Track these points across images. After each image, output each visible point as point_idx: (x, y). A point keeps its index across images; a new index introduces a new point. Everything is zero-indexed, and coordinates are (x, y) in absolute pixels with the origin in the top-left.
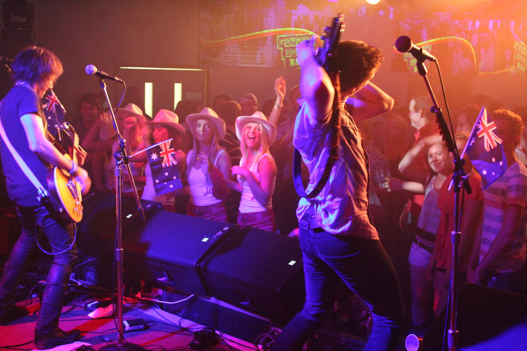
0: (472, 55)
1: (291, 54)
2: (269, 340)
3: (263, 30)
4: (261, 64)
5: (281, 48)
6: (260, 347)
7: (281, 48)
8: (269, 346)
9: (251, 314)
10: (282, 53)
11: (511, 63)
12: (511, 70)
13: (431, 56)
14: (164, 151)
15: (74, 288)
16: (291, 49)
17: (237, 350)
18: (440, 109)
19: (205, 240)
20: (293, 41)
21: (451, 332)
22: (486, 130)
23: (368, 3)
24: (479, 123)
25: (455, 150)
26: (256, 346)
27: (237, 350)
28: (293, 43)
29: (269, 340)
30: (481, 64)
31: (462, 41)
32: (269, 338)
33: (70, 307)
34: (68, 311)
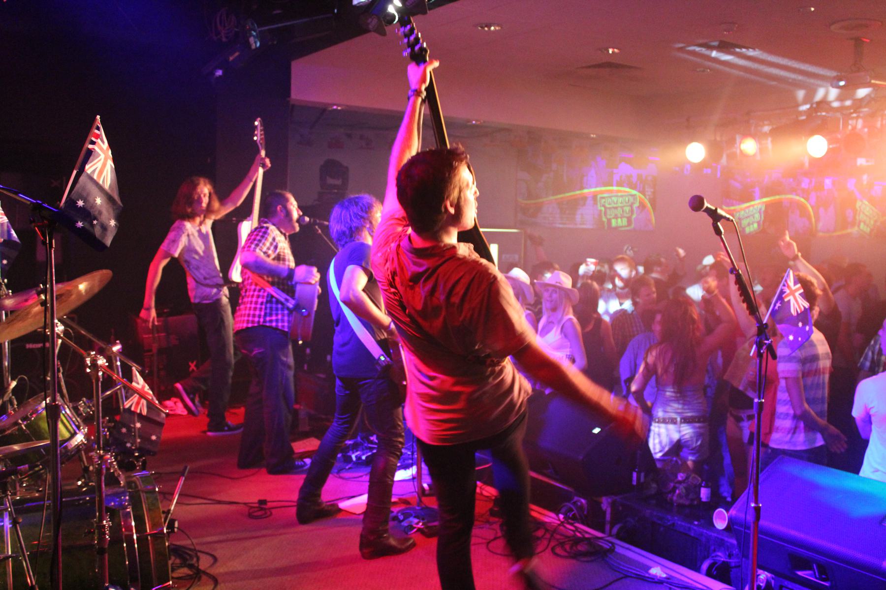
0: (809, 215)
2: (571, 510)
4: (581, 224)
5: (603, 209)
6: (561, 516)
7: (603, 209)
8: (571, 516)
9: (561, 486)
11: (853, 224)
12: (854, 230)
16: (613, 210)
17: (690, 589)
18: (739, 270)
19: (596, 431)
21: (753, 505)
22: (793, 293)
24: (784, 285)
25: (757, 313)
26: (557, 515)
27: (690, 589)
29: (571, 510)
30: (820, 225)
31: (799, 200)
32: (570, 507)
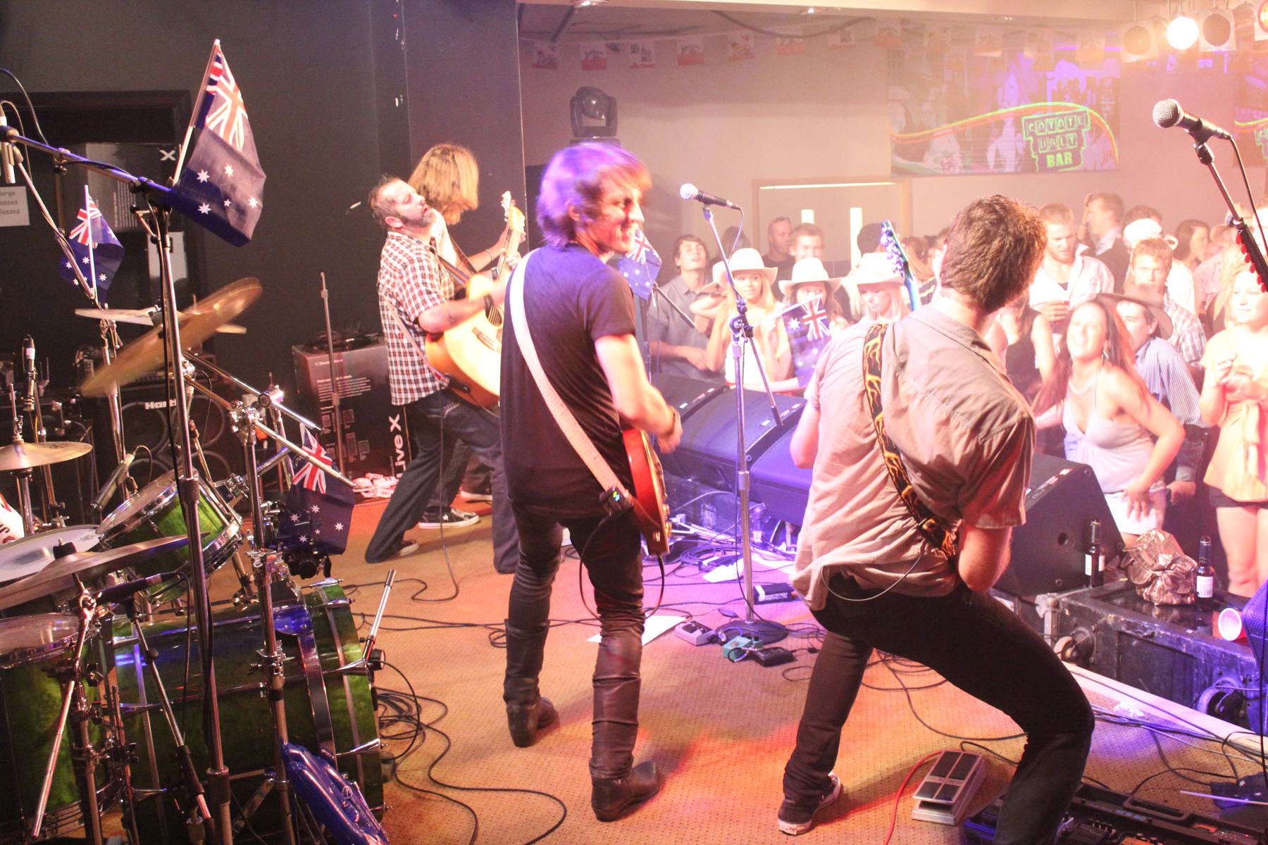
1: (1049, 148)
3: (996, 109)
7: (1031, 139)
10: (1031, 146)
13: (1220, 130)
14: (809, 314)
15: (683, 537)
16: (1047, 139)
20: (1051, 124)
23: (1171, 46)
28: (1052, 127)
33: (679, 564)
34: (674, 571)
